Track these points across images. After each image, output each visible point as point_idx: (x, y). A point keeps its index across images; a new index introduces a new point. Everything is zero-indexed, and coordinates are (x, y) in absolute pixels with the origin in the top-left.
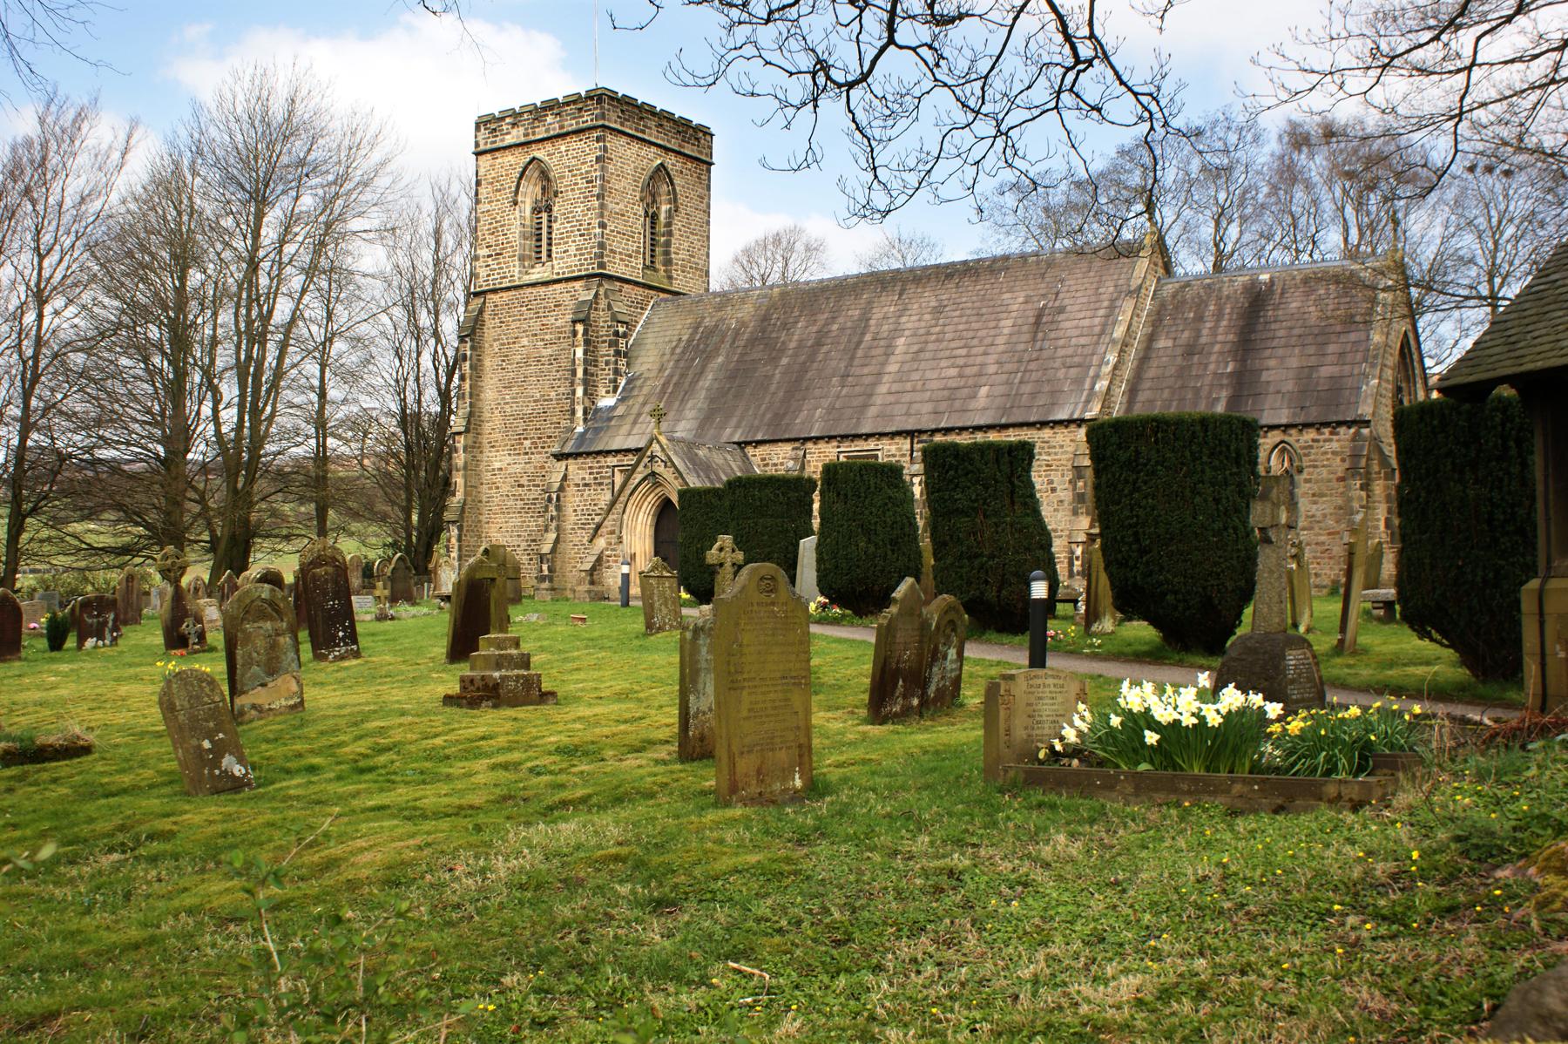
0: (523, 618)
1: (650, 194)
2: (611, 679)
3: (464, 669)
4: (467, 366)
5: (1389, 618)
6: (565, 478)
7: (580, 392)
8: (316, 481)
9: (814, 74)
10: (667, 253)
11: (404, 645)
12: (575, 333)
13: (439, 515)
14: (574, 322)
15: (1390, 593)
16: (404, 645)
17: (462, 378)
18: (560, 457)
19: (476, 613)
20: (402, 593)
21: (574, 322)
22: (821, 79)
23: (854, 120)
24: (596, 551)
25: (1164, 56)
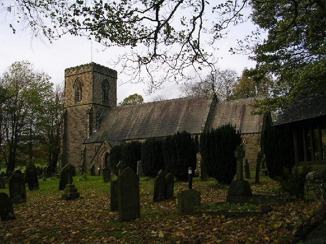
0: (76, 179)
1: (103, 85)
2: (95, 190)
3: (62, 192)
4: (63, 124)
5: (266, 175)
6: (85, 148)
7: (88, 129)
8: (29, 149)
9: (139, 61)
10: (107, 98)
11: (49, 186)
12: (87, 116)
13: (57, 158)
14: (87, 114)
15: (266, 169)
16: (49, 186)
17: (62, 127)
18: (84, 144)
19: (66, 178)
20: (49, 176)
21: (87, 114)
22: (141, 62)
23: (202, 23)
24: (92, 164)
25: (52, 40)
